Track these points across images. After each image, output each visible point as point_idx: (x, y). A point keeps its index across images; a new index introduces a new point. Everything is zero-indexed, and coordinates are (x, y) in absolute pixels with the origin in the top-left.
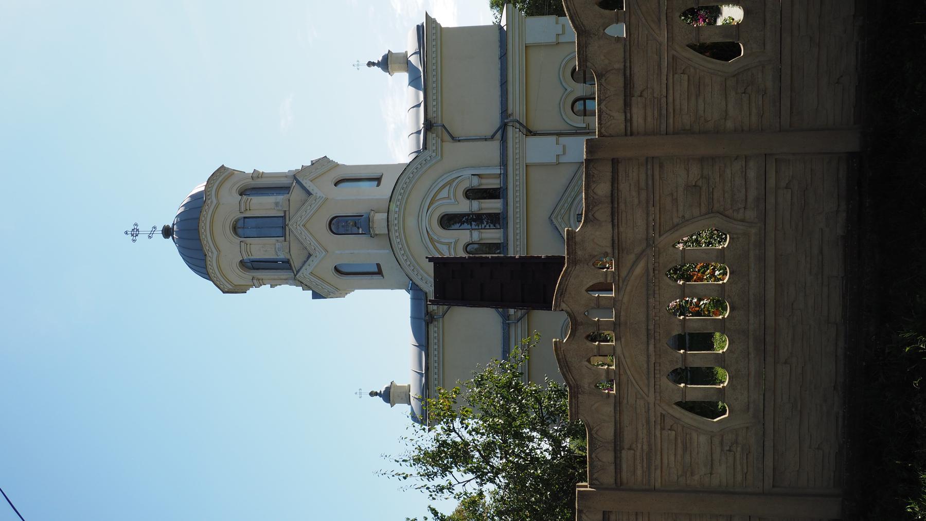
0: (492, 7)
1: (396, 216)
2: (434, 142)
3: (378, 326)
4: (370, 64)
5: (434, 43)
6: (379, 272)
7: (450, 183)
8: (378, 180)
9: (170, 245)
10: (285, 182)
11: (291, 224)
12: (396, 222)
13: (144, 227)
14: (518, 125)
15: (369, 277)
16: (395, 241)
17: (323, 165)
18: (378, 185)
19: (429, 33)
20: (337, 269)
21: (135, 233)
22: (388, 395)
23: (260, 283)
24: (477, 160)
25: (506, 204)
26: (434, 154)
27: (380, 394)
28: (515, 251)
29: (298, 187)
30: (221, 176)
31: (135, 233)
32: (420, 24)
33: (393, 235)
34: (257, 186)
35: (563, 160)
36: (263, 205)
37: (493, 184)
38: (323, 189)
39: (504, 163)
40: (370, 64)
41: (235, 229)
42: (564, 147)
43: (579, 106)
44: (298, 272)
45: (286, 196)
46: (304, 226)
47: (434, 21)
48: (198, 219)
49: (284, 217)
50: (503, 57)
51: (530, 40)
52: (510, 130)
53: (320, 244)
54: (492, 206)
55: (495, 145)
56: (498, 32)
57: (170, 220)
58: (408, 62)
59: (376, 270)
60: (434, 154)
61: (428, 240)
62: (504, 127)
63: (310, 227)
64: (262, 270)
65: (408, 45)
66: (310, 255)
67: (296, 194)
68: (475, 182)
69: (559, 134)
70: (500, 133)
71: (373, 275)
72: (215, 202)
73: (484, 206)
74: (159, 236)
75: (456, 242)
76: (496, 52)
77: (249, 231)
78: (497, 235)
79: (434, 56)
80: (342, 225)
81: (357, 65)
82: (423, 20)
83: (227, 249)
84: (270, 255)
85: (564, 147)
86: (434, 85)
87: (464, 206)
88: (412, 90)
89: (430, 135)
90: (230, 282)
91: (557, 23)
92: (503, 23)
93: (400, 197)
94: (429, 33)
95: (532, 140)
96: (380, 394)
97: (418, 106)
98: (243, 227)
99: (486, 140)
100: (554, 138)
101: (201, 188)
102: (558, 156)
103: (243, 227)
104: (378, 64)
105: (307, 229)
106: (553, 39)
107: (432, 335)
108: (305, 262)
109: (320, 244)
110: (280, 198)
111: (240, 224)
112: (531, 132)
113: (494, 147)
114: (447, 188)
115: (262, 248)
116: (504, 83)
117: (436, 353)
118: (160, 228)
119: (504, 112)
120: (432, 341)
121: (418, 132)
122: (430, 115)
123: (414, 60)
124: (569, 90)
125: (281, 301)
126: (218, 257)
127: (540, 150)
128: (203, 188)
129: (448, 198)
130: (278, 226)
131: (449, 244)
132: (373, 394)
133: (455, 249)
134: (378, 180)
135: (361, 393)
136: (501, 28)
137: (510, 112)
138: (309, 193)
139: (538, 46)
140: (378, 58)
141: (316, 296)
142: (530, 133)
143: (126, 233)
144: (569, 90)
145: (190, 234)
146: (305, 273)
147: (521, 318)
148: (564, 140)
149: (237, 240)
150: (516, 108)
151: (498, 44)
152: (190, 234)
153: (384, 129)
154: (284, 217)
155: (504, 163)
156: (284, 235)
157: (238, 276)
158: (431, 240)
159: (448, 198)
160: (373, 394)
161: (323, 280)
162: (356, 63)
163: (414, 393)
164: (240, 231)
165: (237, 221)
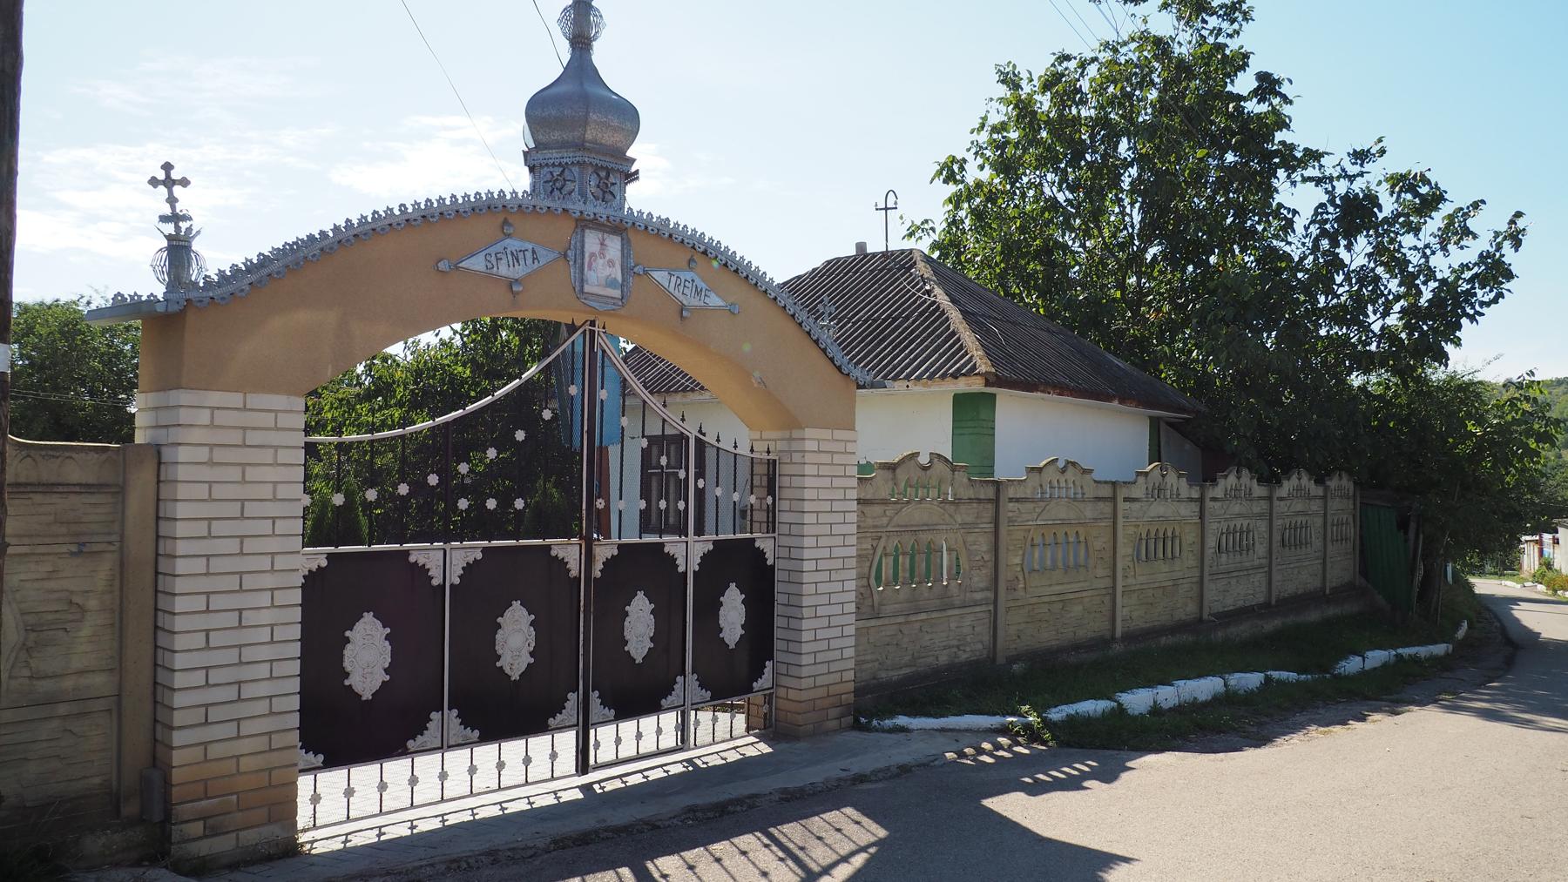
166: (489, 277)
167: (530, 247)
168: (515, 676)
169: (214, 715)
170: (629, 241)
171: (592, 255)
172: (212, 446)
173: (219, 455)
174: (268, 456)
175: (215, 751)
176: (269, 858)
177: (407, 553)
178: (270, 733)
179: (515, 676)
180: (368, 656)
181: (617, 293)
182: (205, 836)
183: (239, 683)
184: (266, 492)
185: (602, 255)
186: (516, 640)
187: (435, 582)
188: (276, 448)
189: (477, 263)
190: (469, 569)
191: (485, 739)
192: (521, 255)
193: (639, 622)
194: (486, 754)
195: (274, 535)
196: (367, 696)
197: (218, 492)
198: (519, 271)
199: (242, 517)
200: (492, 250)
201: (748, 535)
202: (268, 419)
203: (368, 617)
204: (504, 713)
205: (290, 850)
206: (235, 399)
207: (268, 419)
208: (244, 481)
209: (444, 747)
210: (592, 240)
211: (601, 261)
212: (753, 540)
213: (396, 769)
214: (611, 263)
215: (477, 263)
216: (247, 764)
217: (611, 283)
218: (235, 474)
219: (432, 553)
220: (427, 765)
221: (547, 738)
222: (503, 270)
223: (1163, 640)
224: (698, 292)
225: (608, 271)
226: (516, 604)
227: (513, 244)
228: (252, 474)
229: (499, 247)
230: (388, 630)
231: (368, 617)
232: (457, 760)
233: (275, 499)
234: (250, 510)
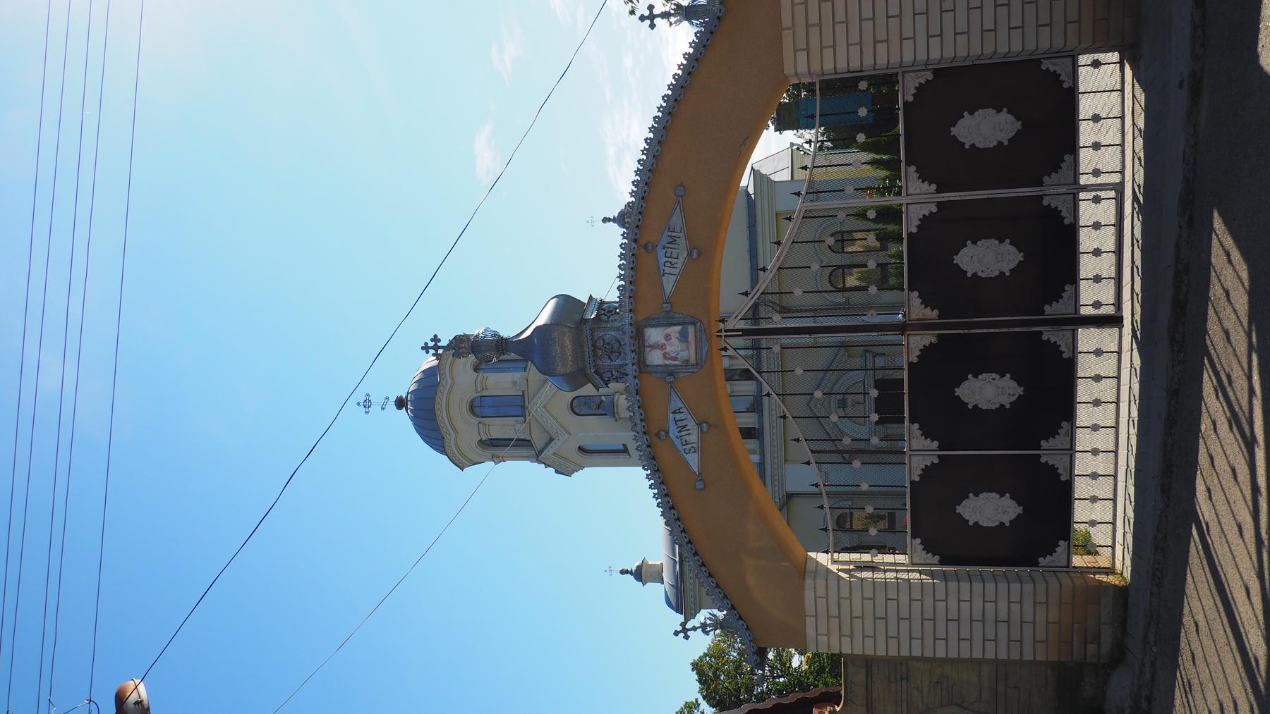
4: (606, 220)
6: (625, 450)
9: (403, 417)
13: (377, 399)
20: (581, 449)
21: (367, 404)
22: (641, 574)
23: (498, 459)
27: (630, 572)
28: (1134, 176)
40: (606, 220)
41: (472, 408)
49: (523, 396)
56: (745, 198)
64: (496, 448)
66: (551, 440)
72: (450, 382)
73: (736, 388)
74: (391, 407)
77: (485, 397)
78: (751, 420)
81: (591, 222)
83: (467, 430)
96: (630, 572)
98: (478, 407)
104: (614, 220)
111: (477, 403)
115: (500, 428)
126: (456, 441)
132: (623, 572)
136: (748, 195)
145: (424, 407)
149: (476, 420)
151: (747, 257)
152: (424, 407)
160: (623, 572)
163: (666, 575)
164: (477, 410)
165: (472, 401)
166: (702, 449)
167: (671, 415)
168: (1020, 391)
169: (1003, 11)
170: (647, 319)
171: (665, 356)
172: (841, 636)
173: (846, 631)
174: (845, 604)
175: (1041, 635)
176: (1125, 605)
177: (906, 104)
178: (1035, 603)
179: (1020, 391)
180: (989, 510)
181: (691, 330)
182: (1099, 644)
183: (996, 621)
184: (868, 604)
185: (662, 347)
186: (986, 258)
187: (936, 461)
188: (839, 598)
189: (693, 460)
190: (926, 434)
191: (1070, 415)
192: (680, 424)
193: (986, 258)
194: (1084, 415)
195: (897, 600)
196: (1020, 510)
197: (870, 632)
198: (691, 425)
199: (886, 619)
200: (681, 448)
201: (908, 491)
202: (821, 602)
203: (957, 259)
204: (1051, 395)
205: (1122, 593)
206: (810, 622)
207: (821, 602)
208: (862, 617)
209: (1071, 450)
210: (655, 358)
211: (669, 348)
212: (911, 364)
213: (1082, 488)
214: (667, 337)
215: (693, 460)
216: (1054, 616)
217: (683, 336)
218: (858, 623)
219: (913, 465)
220: (1083, 464)
221: (1081, 359)
222: (693, 438)
223: (1254, 340)
224: (673, 240)
225: (674, 340)
226: (958, 392)
227: (673, 432)
228: (857, 613)
229: (678, 442)
230: (966, 114)
231: (957, 259)
232: (1084, 440)
233: (874, 599)
234: (881, 613)
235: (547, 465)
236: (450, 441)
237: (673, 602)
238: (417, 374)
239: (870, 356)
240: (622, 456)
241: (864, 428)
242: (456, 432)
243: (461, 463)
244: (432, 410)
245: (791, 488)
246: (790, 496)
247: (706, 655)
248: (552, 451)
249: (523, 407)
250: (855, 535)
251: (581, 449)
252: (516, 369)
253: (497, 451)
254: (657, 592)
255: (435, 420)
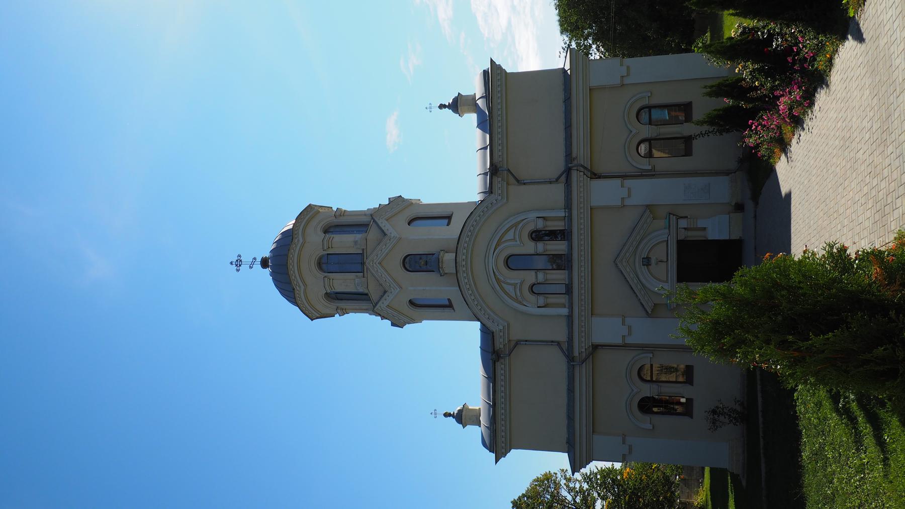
0: (562, 33)
1: (464, 257)
2: (500, 185)
3: (449, 355)
4: (442, 106)
5: (499, 89)
6: (450, 305)
7: (515, 225)
8: (449, 218)
10: (365, 219)
11: (368, 262)
12: (464, 263)
14: (582, 169)
15: (440, 310)
16: (463, 281)
17: (397, 202)
18: (448, 224)
19: (495, 77)
20: (411, 303)
21: (238, 263)
22: (463, 417)
23: (343, 312)
24: (541, 202)
25: (570, 247)
26: (500, 198)
29: (374, 225)
30: (309, 214)
31: (238, 263)
32: (485, 68)
33: (461, 275)
34: (341, 223)
35: (627, 81)
36: (344, 243)
37: (558, 226)
38: (397, 229)
39: (568, 206)
40: (442, 106)
42: (629, 189)
43: (645, 116)
44: (376, 304)
45: (364, 235)
46: (380, 263)
47: (499, 67)
48: (287, 255)
49: (362, 254)
50: (567, 100)
51: (594, 83)
52: (574, 174)
53: (394, 280)
54: (558, 247)
55: (560, 188)
57: (266, 251)
58: (477, 105)
59: (447, 303)
60: (500, 198)
61: (494, 280)
62: (568, 171)
63: (386, 266)
65: (475, 88)
66: (385, 292)
67: (373, 234)
68: (540, 225)
69: (624, 177)
70: (564, 175)
71: (443, 309)
73: (549, 247)
74: (258, 266)
75: (522, 283)
76: (561, 96)
79: (501, 99)
80: (417, 263)
81: (430, 108)
82: (488, 66)
83: (314, 283)
84: (351, 289)
85: (629, 189)
86: (500, 130)
87: (530, 247)
88: (479, 132)
89: (495, 178)
90: (317, 311)
91: (622, 65)
92: (567, 67)
93: (467, 239)
94: (495, 77)
95: (597, 184)
97: (485, 148)
98: (327, 263)
99: (551, 183)
100: (618, 182)
101: (290, 226)
102: (623, 199)
103: (327, 263)
105: (382, 267)
106: (618, 81)
107: (499, 372)
108: (382, 296)
109: (394, 280)
110: (358, 237)
112: (595, 174)
113: (558, 190)
114: (513, 230)
115: (343, 282)
116: (568, 127)
117: (503, 389)
118: (259, 259)
119: (569, 156)
120: (499, 377)
121: (485, 174)
122: (496, 160)
123: (480, 103)
124: (634, 131)
125: (360, 327)
126: (305, 290)
127: (605, 193)
128: (291, 227)
129: (514, 239)
130: (355, 263)
131: (515, 285)
132: (447, 415)
133: (520, 289)
134: (449, 218)
135: (435, 414)
137: (574, 155)
138: (385, 234)
139: (602, 88)
140: (449, 100)
141: (393, 324)
142: (595, 176)
143: (239, 256)
144: (634, 131)
145: (281, 264)
146: (383, 305)
147: (585, 360)
148: (629, 182)
149: (321, 275)
150: (580, 151)
152: (281, 264)
153: (450, 169)
154: (362, 254)
155: (568, 206)
156: (363, 272)
157: (323, 306)
158: (498, 280)
159: (514, 239)
160: (447, 415)
161: (399, 312)
162: (428, 106)
163: (483, 419)
164: (324, 266)
165: (320, 258)
235: (383, 318)
236: (300, 292)
237: (487, 442)
238: (275, 235)
239: (673, 218)
240: (447, 310)
241: (662, 282)
242: (305, 285)
243: (313, 314)
244: (286, 265)
245: (597, 339)
246: (596, 347)
247: (524, 496)
248: (386, 303)
249: (363, 264)
250: (655, 386)
251: (411, 303)
252: (359, 232)
253: (342, 304)
254: (475, 433)
255: (288, 274)
